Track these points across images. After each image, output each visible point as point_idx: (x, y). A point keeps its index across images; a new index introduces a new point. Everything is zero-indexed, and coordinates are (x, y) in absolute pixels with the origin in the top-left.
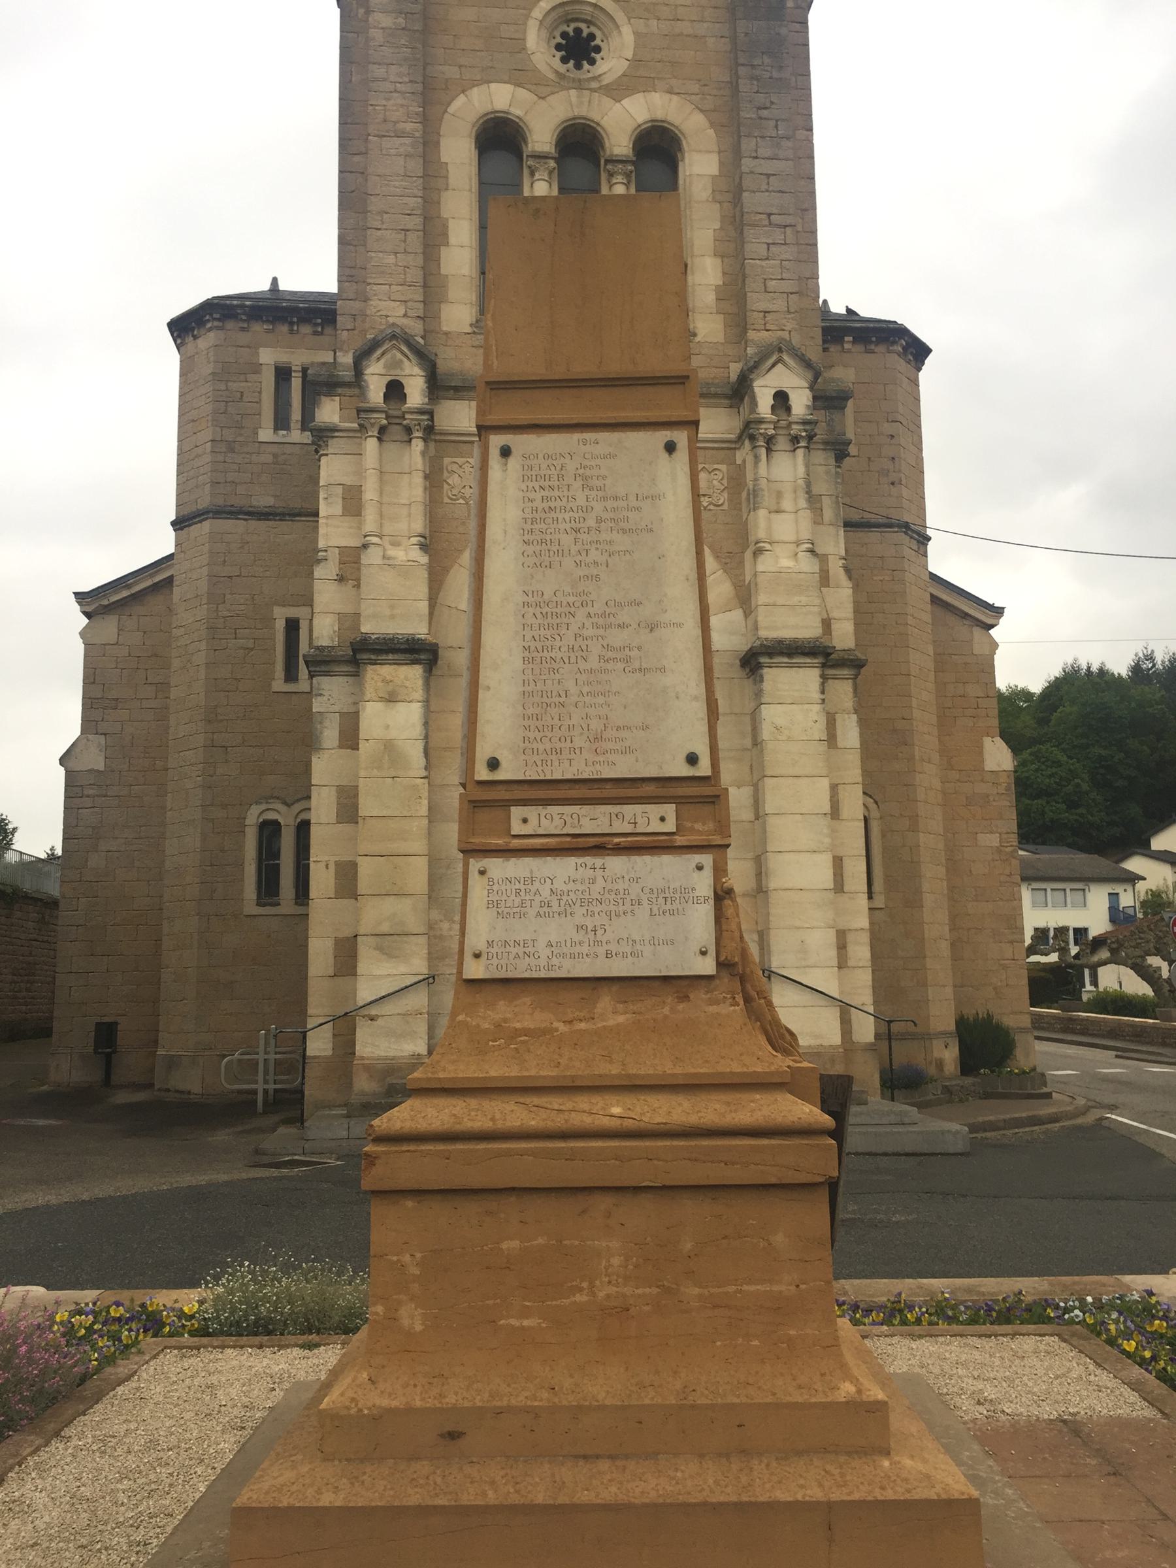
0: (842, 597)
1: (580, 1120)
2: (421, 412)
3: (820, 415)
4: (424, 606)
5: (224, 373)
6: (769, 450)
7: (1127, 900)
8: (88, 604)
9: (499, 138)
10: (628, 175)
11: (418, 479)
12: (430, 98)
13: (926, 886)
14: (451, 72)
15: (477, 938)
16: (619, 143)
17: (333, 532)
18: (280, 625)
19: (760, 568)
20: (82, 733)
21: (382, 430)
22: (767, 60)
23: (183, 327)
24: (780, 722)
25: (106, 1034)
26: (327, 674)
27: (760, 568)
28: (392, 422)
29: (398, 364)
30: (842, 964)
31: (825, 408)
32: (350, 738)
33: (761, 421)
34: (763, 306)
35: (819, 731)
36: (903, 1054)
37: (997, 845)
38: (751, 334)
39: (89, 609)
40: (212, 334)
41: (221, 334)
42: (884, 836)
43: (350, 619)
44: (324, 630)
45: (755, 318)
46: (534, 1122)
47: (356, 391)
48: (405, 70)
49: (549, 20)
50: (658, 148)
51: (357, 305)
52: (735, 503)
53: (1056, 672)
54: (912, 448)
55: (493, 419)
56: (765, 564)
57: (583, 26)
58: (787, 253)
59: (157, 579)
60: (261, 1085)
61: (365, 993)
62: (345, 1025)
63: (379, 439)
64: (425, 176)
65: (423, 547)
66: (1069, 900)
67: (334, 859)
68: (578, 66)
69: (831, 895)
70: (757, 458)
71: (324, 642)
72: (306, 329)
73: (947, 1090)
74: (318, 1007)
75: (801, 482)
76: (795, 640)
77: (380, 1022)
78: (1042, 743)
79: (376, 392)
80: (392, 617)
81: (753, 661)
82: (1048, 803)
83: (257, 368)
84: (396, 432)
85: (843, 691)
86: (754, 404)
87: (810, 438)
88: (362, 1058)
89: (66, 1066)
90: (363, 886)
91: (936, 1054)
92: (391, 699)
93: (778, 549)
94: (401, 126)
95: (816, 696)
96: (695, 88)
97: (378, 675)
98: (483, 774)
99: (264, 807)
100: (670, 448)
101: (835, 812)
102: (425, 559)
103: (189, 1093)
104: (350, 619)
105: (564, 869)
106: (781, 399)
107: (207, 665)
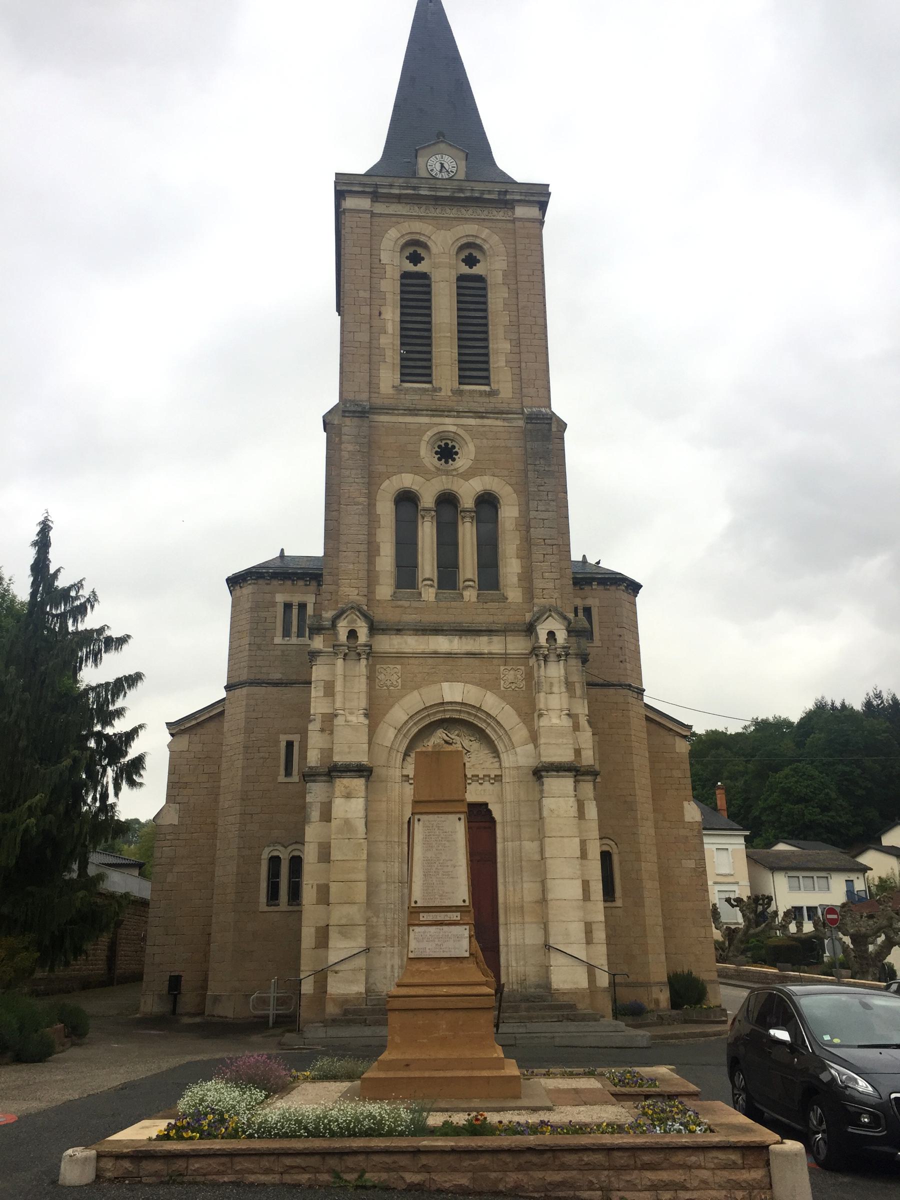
0: (586, 737)
1: (438, 993)
2: (366, 646)
3: (573, 640)
4: (366, 746)
5: (256, 607)
6: (545, 661)
7: (859, 885)
8: (174, 729)
9: (406, 500)
10: (472, 518)
11: (364, 680)
12: (372, 482)
13: (646, 894)
14: (382, 468)
15: (411, 948)
16: (467, 502)
17: (318, 706)
18: (283, 745)
19: (541, 724)
20: (167, 802)
21: (345, 655)
22: (542, 461)
23: (234, 582)
24: (553, 807)
25: (175, 983)
26: (314, 781)
27: (541, 724)
28: (351, 651)
29: (354, 621)
30: (589, 941)
31: (577, 636)
32: (326, 816)
33: (541, 647)
34: (541, 586)
35: (573, 811)
36: (627, 996)
37: (694, 866)
38: (536, 601)
39: (174, 732)
40: (251, 587)
41: (256, 587)
42: (621, 864)
43: (328, 752)
44: (313, 758)
45: (537, 592)
46: (426, 993)
47: (332, 632)
48: (359, 471)
49: (432, 440)
50: (488, 503)
51: (333, 587)
52: (529, 687)
53: (810, 706)
54: (632, 640)
55: (416, 811)
56: (544, 722)
57: (449, 442)
58: (554, 559)
59: (211, 714)
60: (271, 1011)
61: (333, 958)
62: (321, 977)
63: (344, 659)
64: (369, 505)
65: (366, 715)
66: (816, 886)
67: (316, 882)
68: (447, 462)
69: (581, 903)
70: (539, 666)
71: (313, 764)
72: (301, 583)
73: (661, 1017)
74: (306, 967)
75: (562, 678)
76: (560, 763)
77: (340, 974)
78: (799, 761)
79: (343, 636)
80: (349, 753)
81: (540, 772)
82: (806, 807)
83: (274, 604)
84: (353, 655)
85: (587, 788)
86: (537, 638)
87: (567, 655)
88: (331, 995)
89: (150, 1003)
90: (332, 900)
91: (654, 996)
92: (348, 796)
93: (550, 713)
94: (357, 500)
95: (572, 793)
96: (506, 473)
97: (343, 784)
98: (413, 905)
99: (272, 848)
100: (460, 819)
101: (584, 855)
102: (367, 722)
103: (226, 1017)
104: (328, 752)
105: (433, 929)
106: (551, 635)
107: (243, 768)
